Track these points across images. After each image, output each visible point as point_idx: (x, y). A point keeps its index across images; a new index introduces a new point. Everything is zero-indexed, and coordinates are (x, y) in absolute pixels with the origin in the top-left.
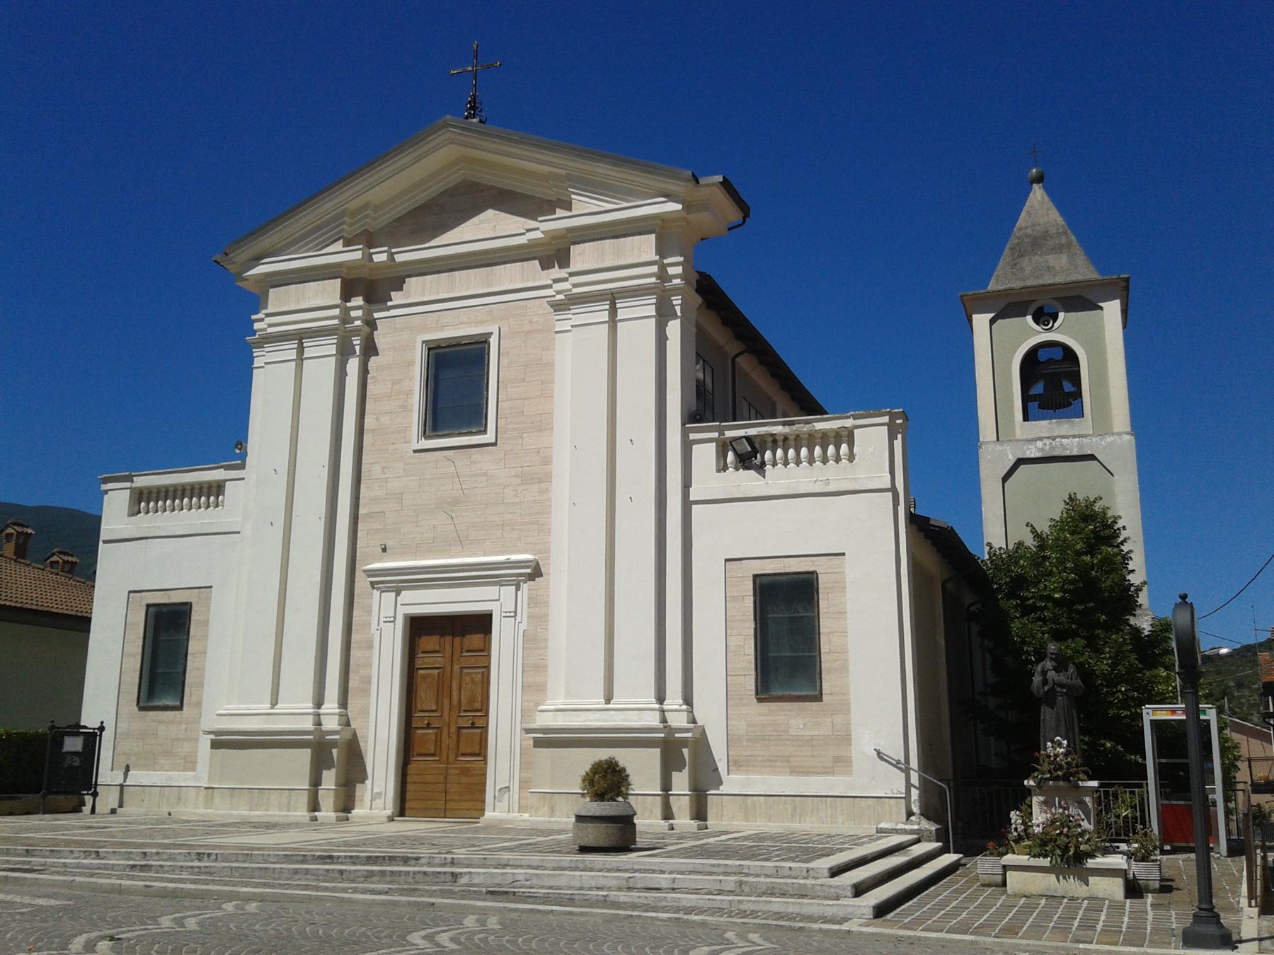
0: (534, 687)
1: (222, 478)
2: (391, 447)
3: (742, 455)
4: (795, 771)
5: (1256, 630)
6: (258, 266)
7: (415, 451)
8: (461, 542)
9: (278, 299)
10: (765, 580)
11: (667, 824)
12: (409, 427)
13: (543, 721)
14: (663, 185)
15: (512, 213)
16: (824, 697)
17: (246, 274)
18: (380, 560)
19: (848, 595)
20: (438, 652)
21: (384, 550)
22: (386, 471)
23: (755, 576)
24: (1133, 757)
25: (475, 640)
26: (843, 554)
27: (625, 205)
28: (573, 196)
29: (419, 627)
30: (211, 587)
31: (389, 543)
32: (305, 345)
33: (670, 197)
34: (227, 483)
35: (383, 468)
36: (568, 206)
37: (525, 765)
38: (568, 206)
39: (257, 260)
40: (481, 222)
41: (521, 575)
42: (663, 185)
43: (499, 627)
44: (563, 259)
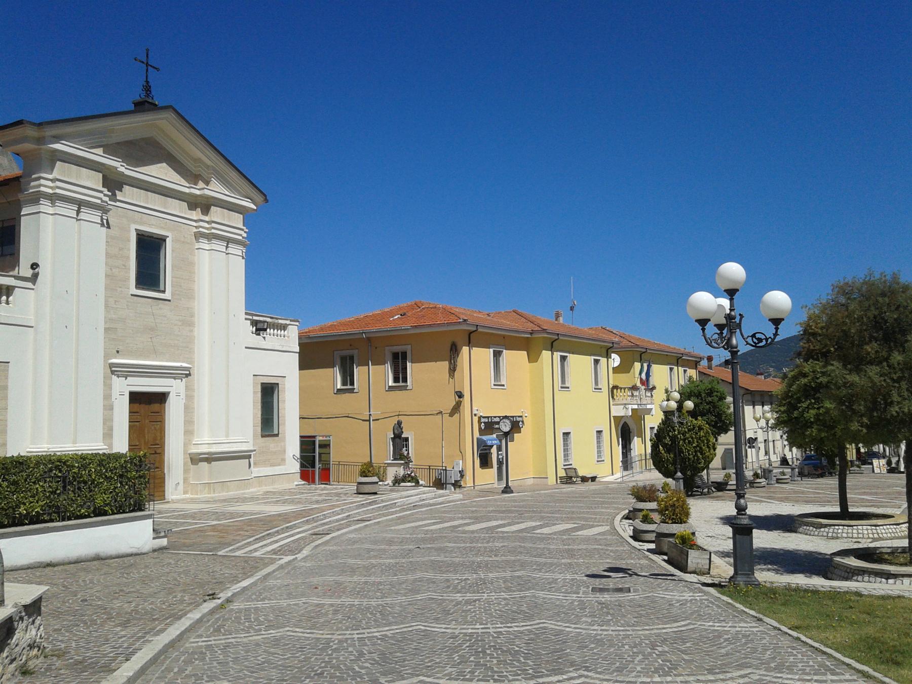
0: (189, 432)
1: (14, 285)
2: (119, 289)
3: (14, 289)
4: (272, 465)
5: (774, 441)
6: (57, 143)
7: (132, 295)
8: (154, 353)
9: (60, 170)
10: (265, 385)
11: (663, 481)
12: (128, 279)
13: (194, 450)
14: (252, 194)
15: (174, 170)
16: (280, 435)
17: (51, 146)
18: (115, 358)
19: (286, 394)
20: (138, 412)
21: (118, 352)
22: (117, 303)
23: (262, 384)
24: (838, 463)
25: (155, 407)
26: (285, 377)
27: (233, 195)
28: (212, 179)
29: (136, 398)
30: (9, 362)
31: (121, 348)
32: (82, 210)
33: (253, 202)
34: (16, 289)
35: (116, 301)
36: (207, 183)
37: (186, 471)
38: (207, 183)
39: (57, 138)
40: (161, 168)
41: (182, 374)
42: (252, 194)
43: (171, 400)
44: (206, 210)
